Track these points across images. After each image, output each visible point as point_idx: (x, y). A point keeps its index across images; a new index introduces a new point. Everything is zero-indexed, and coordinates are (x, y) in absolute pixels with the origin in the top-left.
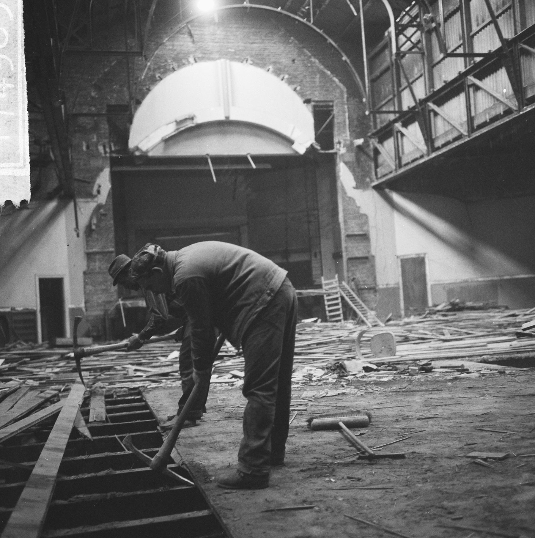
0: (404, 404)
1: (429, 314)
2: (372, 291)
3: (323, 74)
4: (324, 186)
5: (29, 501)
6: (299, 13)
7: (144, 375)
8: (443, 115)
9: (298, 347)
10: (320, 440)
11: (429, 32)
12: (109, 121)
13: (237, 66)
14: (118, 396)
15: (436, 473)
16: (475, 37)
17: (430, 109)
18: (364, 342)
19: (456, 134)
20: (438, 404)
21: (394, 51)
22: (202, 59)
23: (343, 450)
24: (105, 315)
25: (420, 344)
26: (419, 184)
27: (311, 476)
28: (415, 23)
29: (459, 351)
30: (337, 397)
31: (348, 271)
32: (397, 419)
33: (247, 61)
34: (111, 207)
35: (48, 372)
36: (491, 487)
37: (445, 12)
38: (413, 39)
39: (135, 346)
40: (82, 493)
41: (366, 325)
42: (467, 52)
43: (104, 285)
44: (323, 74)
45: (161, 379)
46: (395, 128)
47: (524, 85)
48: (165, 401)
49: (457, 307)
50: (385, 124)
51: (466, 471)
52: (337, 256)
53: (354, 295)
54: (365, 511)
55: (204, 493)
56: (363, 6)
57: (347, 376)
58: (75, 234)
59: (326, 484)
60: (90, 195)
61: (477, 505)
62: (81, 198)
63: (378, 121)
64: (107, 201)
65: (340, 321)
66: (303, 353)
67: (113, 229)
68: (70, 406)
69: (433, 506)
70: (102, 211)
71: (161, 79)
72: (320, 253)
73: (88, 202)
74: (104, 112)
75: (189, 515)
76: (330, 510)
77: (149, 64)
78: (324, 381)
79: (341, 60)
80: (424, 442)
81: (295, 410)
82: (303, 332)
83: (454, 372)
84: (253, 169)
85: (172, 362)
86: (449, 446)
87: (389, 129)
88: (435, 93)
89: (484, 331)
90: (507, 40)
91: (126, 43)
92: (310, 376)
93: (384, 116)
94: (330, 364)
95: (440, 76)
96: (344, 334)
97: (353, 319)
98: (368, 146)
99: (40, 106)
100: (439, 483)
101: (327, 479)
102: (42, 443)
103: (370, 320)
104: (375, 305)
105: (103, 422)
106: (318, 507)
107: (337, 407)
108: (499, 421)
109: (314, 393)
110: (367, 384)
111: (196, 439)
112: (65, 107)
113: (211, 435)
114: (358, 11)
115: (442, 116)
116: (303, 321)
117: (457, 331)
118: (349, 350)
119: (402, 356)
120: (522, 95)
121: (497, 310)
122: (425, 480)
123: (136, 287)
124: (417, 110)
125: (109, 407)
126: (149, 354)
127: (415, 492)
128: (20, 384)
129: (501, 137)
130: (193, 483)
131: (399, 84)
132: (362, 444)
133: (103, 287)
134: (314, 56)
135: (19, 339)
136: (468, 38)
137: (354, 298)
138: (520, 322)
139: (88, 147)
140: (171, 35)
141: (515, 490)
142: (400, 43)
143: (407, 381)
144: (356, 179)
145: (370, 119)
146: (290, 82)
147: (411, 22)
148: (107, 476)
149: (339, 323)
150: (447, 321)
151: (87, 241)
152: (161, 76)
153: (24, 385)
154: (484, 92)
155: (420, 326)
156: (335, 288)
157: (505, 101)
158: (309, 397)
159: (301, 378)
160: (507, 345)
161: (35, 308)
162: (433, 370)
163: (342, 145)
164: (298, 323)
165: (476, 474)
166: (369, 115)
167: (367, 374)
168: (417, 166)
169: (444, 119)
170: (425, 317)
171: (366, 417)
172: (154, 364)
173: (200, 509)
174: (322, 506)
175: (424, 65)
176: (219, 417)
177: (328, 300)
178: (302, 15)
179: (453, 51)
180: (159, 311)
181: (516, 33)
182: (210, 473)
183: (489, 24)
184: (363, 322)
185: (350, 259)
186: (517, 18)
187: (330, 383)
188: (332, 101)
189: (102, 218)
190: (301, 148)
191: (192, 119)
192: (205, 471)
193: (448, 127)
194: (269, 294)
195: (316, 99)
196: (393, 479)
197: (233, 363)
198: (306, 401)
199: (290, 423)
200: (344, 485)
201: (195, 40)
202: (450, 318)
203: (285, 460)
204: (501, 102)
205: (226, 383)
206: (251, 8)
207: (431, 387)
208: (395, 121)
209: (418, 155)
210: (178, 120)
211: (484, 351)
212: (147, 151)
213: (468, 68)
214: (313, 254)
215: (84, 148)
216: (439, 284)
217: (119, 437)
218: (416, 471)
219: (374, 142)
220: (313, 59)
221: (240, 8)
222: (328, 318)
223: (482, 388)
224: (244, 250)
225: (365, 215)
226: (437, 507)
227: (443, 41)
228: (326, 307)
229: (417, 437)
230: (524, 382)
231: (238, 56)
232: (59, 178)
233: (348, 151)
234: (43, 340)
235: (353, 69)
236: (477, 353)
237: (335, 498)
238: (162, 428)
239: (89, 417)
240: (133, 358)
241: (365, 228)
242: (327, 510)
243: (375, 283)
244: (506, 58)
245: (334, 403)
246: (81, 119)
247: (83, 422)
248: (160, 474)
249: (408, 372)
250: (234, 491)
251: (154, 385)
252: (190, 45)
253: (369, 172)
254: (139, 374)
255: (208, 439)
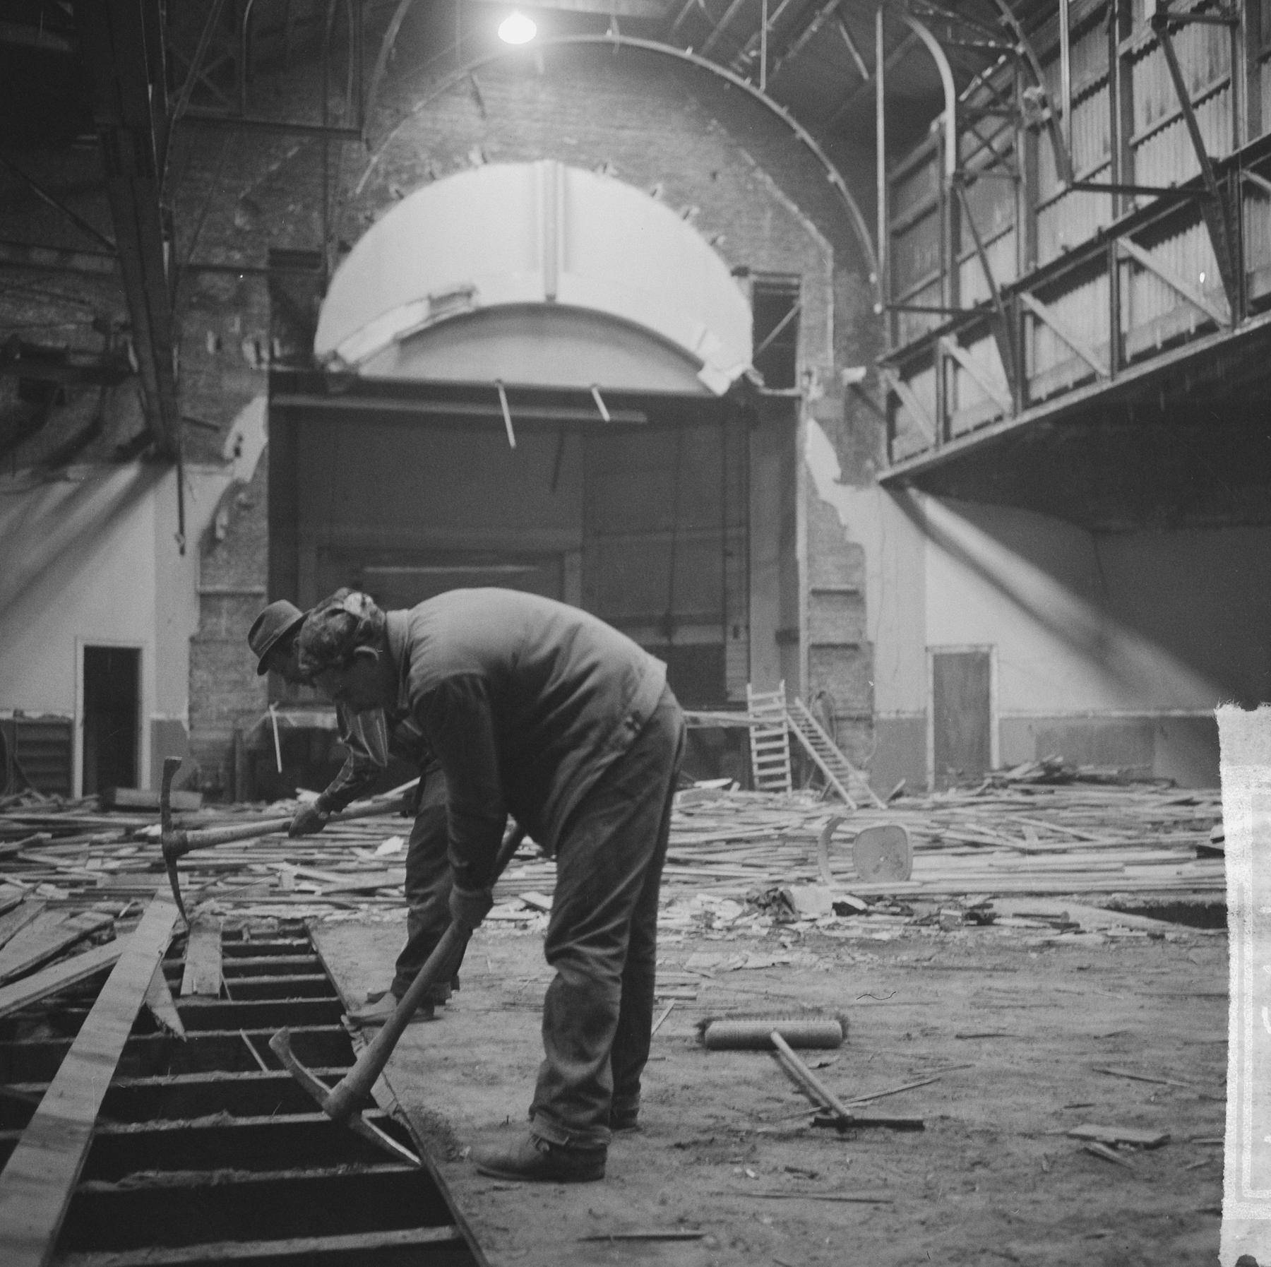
0: (927, 997)
1: (992, 785)
2: (862, 725)
3: (781, 211)
4: (766, 472)
5: (27, 1179)
6: (734, 65)
7: (319, 890)
8: (1055, 326)
9: (674, 846)
10: (725, 1072)
11: (1035, 130)
12: (274, 287)
13: (581, 178)
14: (253, 937)
15: (995, 1171)
16: (1141, 148)
17: (1026, 308)
18: (837, 844)
19: (1081, 372)
20: (1006, 1003)
21: (950, 167)
22: (500, 157)
23: (780, 1101)
24: (234, 742)
25: (968, 858)
26: (992, 480)
27: (699, 1159)
28: (1003, 107)
29: (1063, 880)
30: (768, 972)
31: (809, 674)
32: (908, 1035)
33: (605, 167)
34: (264, 489)
35: (89, 868)
36: (1125, 1212)
37: (1075, 86)
38: (996, 145)
39: (308, 825)
40: (152, 1167)
41: (845, 803)
42: (1120, 182)
43: (236, 670)
44: (781, 211)
45: (358, 903)
46: (940, 347)
47: (1248, 267)
48: (363, 957)
49: (1057, 775)
50: (917, 337)
51: (1067, 1169)
52: (787, 637)
53: (821, 732)
54: (823, 1253)
55: (444, 1185)
56: (885, 58)
57: (793, 922)
58: (176, 548)
59: (734, 1182)
60: (216, 458)
61: (1089, 1254)
62: (196, 462)
63: (903, 328)
64: (255, 476)
65: (784, 789)
66: (694, 861)
67: (266, 540)
68: (135, 959)
69: (984, 1251)
70: (242, 496)
71: (401, 197)
72: (747, 627)
73: (210, 473)
74: (262, 264)
75: (404, 1237)
76: (741, 1246)
77: (375, 159)
78: (740, 932)
79: (826, 181)
80: (970, 1092)
81: (668, 998)
82: (697, 811)
83: (1045, 927)
84: (602, 422)
85: (384, 862)
86: (1027, 1107)
87: (925, 349)
88: (1039, 274)
89: (1116, 836)
90: (1214, 161)
91: (325, 107)
92: (707, 919)
93: (916, 318)
94: (758, 890)
95: (1054, 236)
96: (791, 821)
97: (815, 789)
98: (876, 385)
99: (112, 240)
100: (1001, 1196)
101: (737, 1170)
102: (65, 1040)
103: (854, 793)
104: (867, 759)
105: (214, 996)
106: (715, 1237)
107: (767, 996)
108: (1146, 1052)
109: (716, 958)
110: (840, 945)
111: (432, 1052)
112: (172, 247)
113: (468, 1044)
114: (872, 70)
115: (1051, 328)
116: (698, 784)
117: (1053, 831)
118: (802, 862)
119: (924, 883)
120: (1241, 290)
121: (1152, 788)
122: (969, 1187)
123: (307, 680)
124: (994, 309)
125: (231, 961)
126: (334, 840)
127: (943, 1215)
128: (25, 894)
129: (1188, 385)
130: (416, 1159)
131: (957, 247)
132: (825, 1089)
133: (234, 676)
134: (763, 166)
135: (28, 786)
136: (1126, 148)
137: (818, 738)
138: (1202, 820)
139: (219, 345)
140: (432, 96)
141: (1182, 1224)
142: (965, 152)
143: (935, 943)
144: (842, 460)
145: (883, 322)
146: (703, 224)
147: (994, 102)
148: (216, 1130)
149: (781, 795)
150: (1033, 806)
151: (204, 566)
152: (403, 191)
153: (32, 897)
154: (1152, 278)
155: (969, 814)
156: (776, 712)
157: (1202, 302)
158: (704, 968)
159: (687, 920)
160: (1171, 871)
161: (71, 716)
162: (996, 921)
163: (815, 379)
164: (681, 789)
165: (1089, 1178)
166: (882, 314)
167: (841, 920)
168: (986, 440)
169: (1056, 334)
170: (980, 795)
171: (836, 1026)
172: (342, 866)
173: (431, 1223)
174: (723, 1235)
175: (1017, 203)
176: (488, 1003)
177: (760, 740)
178: (740, 70)
179: (1087, 178)
180: (370, 744)
181: (1236, 146)
182: (461, 1138)
183: (1175, 120)
184: (837, 794)
185: (816, 647)
186: (1240, 111)
187: (753, 937)
188: (798, 276)
189: (243, 513)
190: (718, 381)
191: (469, 294)
192: (448, 1133)
193: (1064, 355)
194: (630, 726)
195: (762, 268)
196: (892, 1179)
197: (527, 873)
198: (695, 977)
199: (653, 1030)
200: (778, 1187)
201: (488, 111)
202: (1039, 799)
203: (640, 1118)
204: (1192, 303)
205: (509, 920)
206: (623, 45)
207: (989, 962)
208: (942, 331)
209: (989, 415)
210: (436, 295)
211: (1116, 883)
212: (358, 364)
213: (1121, 218)
214: (730, 629)
215: (211, 347)
216: (1018, 719)
217: (250, 1037)
218: (950, 1163)
219: (889, 378)
220: (759, 174)
221: (596, 44)
222: (756, 781)
223: (1110, 970)
224: (572, 614)
225: (858, 547)
226: (994, 1254)
227: (1065, 152)
228: (754, 755)
229: (953, 1079)
230: (1208, 963)
231: (584, 156)
232: (148, 414)
233: (827, 394)
234: (85, 793)
235: (851, 203)
236: (1100, 885)
237: (755, 1216)
238: (353, 1020)
239: (181, 984)
240: (294, 847)
241: (856, 577)
242: (733, 1245)
243: (872, 708)
244: (1205, 201)
245: (761, 985)
246: (207, 279)
247: (166, 995)
248: (342, 1135)
249: (938, 922)
250: (517, 1184)
251: (340, 915)
252: (476, 122)
253: (874, 447)
254: (305, 885)
255: (459, 1055)
